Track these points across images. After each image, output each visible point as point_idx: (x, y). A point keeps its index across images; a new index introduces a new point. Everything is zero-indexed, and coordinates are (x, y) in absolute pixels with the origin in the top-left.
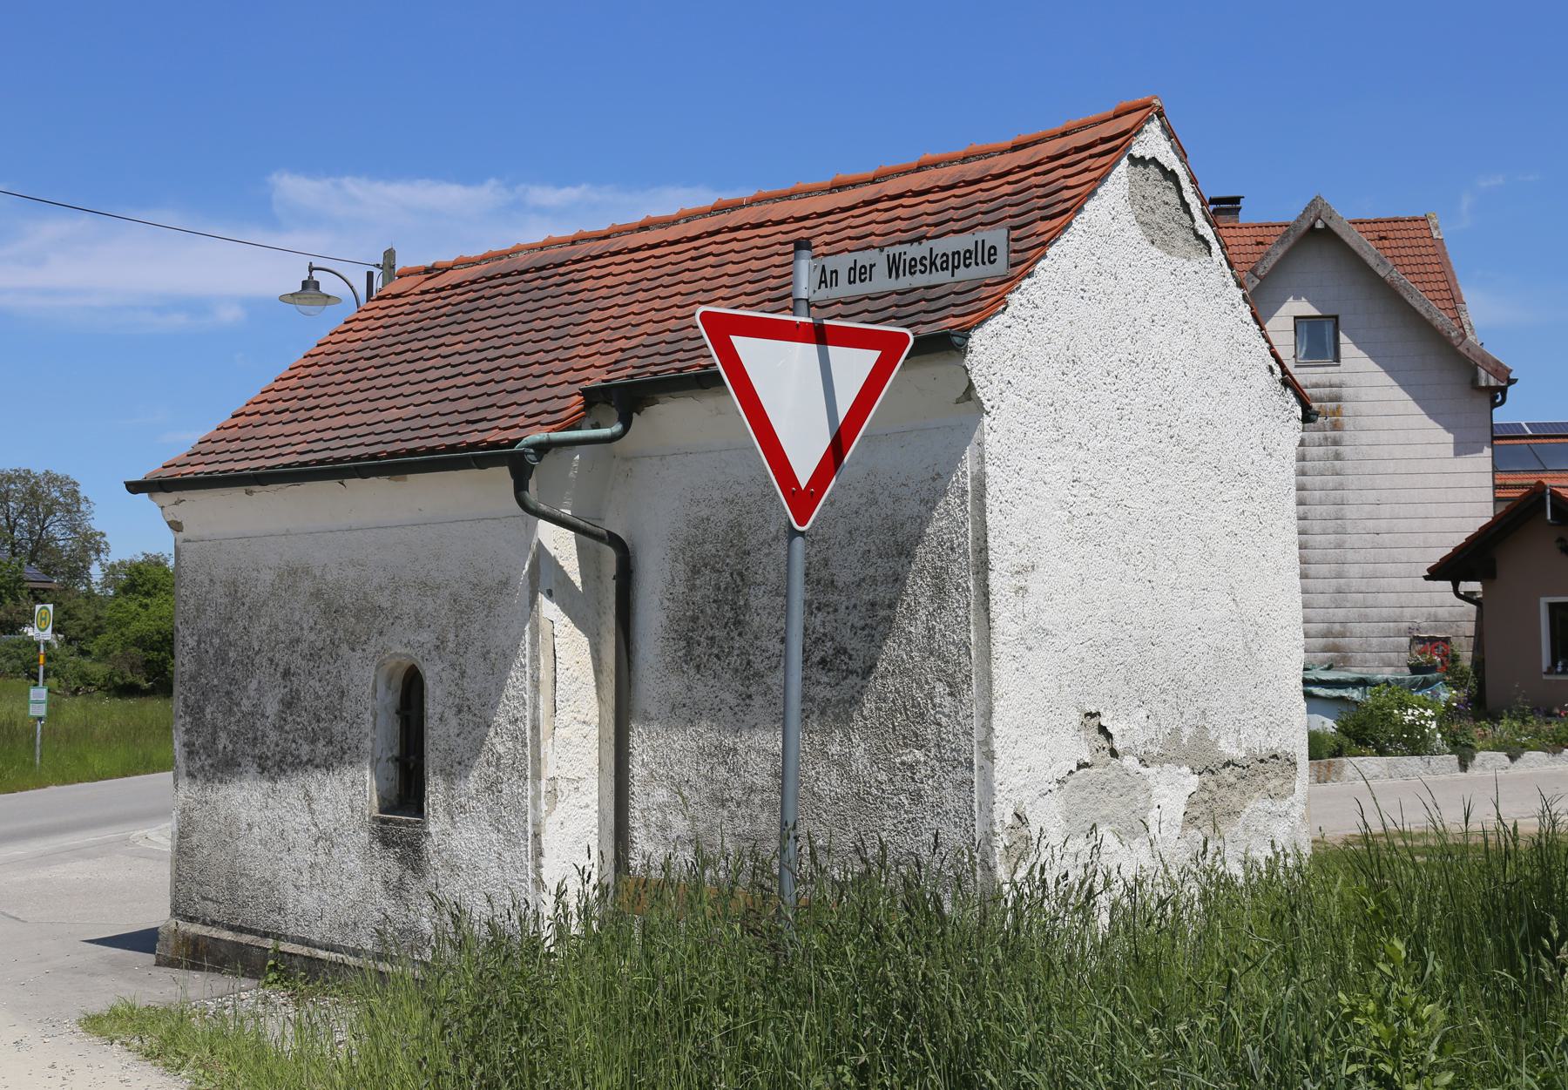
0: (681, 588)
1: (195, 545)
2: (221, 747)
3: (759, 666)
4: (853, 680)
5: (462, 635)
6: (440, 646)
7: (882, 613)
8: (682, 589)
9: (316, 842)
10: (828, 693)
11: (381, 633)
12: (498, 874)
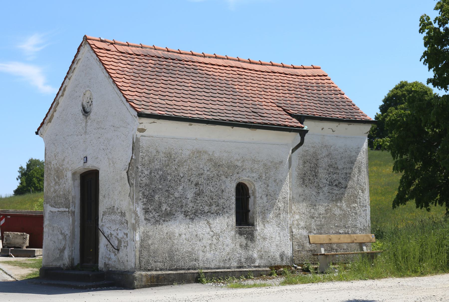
0: (301, 167)
1: (146, 138)
2: (164, 209)
3: (321, 185)
4: (343, 189)
5: (267, 175)
6: (260, 177)
7: (348, 175)
8: (301, 167)
9: (212, 237)
10: (337, 192)
11: (238, 173)
12: (279, 238)
